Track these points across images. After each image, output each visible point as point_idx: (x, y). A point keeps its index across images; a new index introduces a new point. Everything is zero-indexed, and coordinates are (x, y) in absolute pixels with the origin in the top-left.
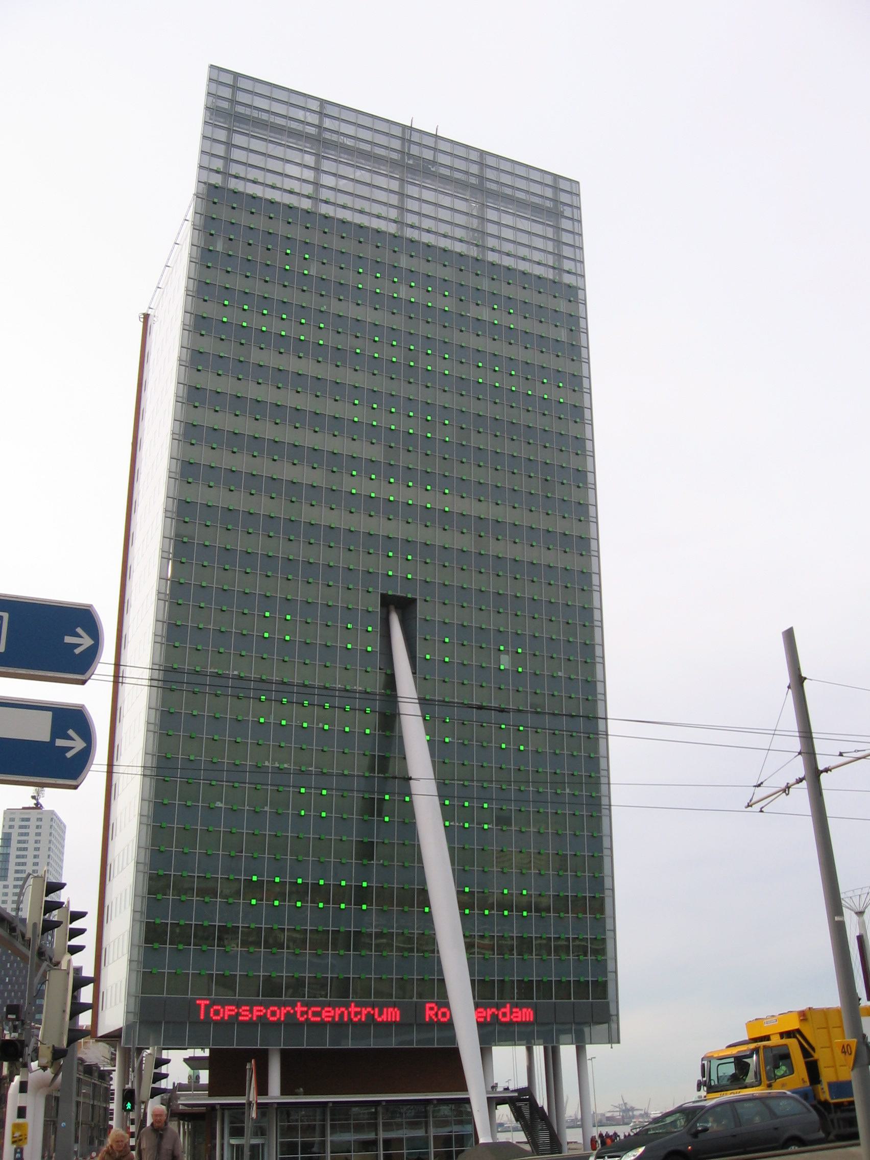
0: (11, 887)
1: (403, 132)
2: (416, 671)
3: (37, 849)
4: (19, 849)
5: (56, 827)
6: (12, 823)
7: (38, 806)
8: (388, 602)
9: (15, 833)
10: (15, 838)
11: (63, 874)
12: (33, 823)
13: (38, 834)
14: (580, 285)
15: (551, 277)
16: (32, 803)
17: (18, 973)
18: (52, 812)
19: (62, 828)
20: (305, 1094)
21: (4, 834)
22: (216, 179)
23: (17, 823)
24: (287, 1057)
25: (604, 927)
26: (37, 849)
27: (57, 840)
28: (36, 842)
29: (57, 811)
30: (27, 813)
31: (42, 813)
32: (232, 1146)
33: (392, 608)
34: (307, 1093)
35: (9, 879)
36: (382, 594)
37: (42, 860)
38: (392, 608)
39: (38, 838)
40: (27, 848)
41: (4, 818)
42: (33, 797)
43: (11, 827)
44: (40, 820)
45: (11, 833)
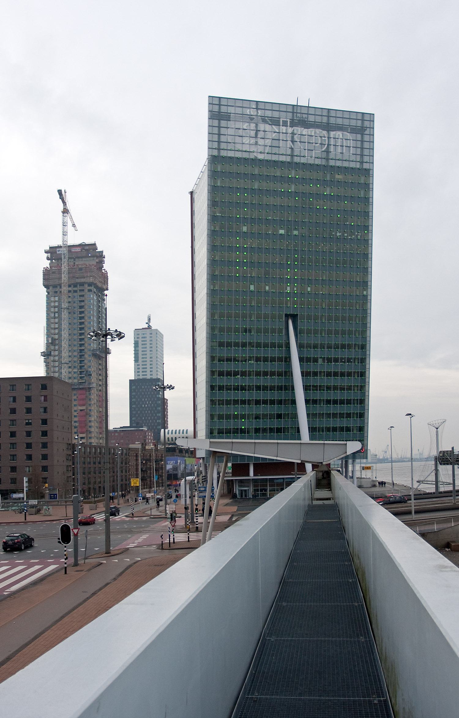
0: (141, 365)
1: (293, 109)
2: (297, 339)
3: (151, 368)
4: (143, 348)
5: (159, 360)
6: (138, 336)
7: (149, 327)
8: (287, 316)
9: (140, 340)
10: (140, 343)
11: (164, 341)
12: (148, 336)
13: (151, 368)
14: (371, 168)
15: (358, 167)
16: (146, 326)
17: (147, 390)
18: (157, 330)
19: (162, 336)
20: (260, 476)
21: (135, 341)
22: (215, 153)
23: (140, 336)
24: (254, 464)
25: (365, 408)
26: (151, 361)
27: (160, 342)
28: (151, 365)
29: (159, 329)
30: (144, 331)
31: (152, 331)
32: (239, 490)
33: (289, 317)
34: (261, 476)
35: (139, 361)
36: (285, 314)
37: (154, 370)
38: (289, 317)
39: (151, 370)
40: (146, 340)
41: (134, 334)
42: (147, 323)
43: (138, 338)
44: (151, 334)
45: (138, 341)
